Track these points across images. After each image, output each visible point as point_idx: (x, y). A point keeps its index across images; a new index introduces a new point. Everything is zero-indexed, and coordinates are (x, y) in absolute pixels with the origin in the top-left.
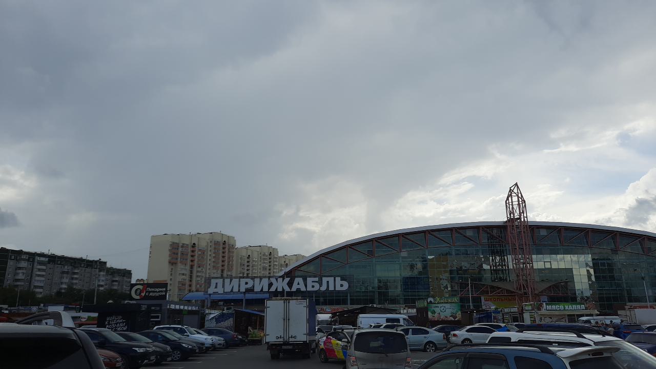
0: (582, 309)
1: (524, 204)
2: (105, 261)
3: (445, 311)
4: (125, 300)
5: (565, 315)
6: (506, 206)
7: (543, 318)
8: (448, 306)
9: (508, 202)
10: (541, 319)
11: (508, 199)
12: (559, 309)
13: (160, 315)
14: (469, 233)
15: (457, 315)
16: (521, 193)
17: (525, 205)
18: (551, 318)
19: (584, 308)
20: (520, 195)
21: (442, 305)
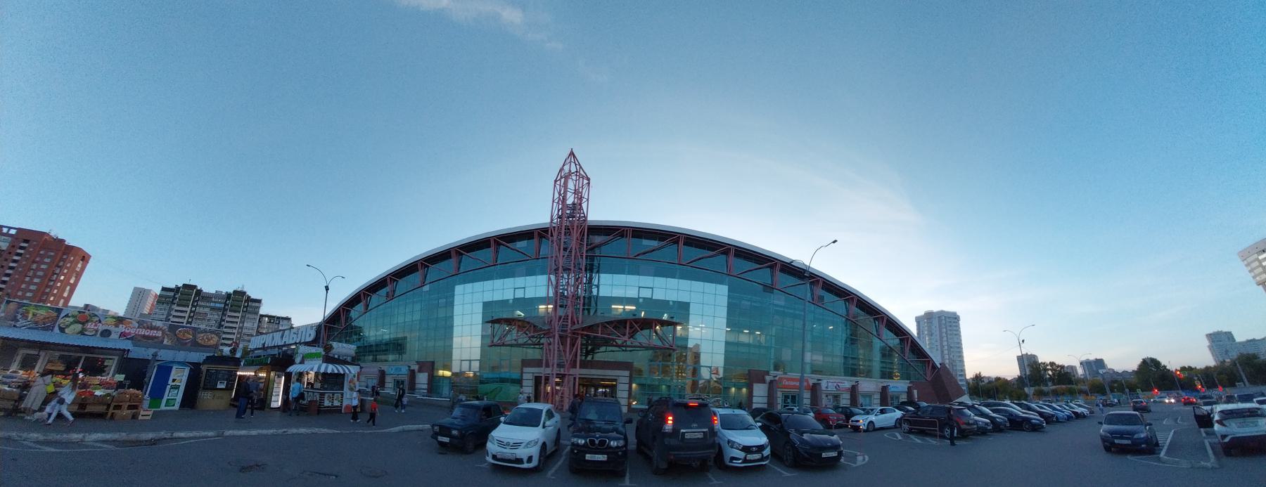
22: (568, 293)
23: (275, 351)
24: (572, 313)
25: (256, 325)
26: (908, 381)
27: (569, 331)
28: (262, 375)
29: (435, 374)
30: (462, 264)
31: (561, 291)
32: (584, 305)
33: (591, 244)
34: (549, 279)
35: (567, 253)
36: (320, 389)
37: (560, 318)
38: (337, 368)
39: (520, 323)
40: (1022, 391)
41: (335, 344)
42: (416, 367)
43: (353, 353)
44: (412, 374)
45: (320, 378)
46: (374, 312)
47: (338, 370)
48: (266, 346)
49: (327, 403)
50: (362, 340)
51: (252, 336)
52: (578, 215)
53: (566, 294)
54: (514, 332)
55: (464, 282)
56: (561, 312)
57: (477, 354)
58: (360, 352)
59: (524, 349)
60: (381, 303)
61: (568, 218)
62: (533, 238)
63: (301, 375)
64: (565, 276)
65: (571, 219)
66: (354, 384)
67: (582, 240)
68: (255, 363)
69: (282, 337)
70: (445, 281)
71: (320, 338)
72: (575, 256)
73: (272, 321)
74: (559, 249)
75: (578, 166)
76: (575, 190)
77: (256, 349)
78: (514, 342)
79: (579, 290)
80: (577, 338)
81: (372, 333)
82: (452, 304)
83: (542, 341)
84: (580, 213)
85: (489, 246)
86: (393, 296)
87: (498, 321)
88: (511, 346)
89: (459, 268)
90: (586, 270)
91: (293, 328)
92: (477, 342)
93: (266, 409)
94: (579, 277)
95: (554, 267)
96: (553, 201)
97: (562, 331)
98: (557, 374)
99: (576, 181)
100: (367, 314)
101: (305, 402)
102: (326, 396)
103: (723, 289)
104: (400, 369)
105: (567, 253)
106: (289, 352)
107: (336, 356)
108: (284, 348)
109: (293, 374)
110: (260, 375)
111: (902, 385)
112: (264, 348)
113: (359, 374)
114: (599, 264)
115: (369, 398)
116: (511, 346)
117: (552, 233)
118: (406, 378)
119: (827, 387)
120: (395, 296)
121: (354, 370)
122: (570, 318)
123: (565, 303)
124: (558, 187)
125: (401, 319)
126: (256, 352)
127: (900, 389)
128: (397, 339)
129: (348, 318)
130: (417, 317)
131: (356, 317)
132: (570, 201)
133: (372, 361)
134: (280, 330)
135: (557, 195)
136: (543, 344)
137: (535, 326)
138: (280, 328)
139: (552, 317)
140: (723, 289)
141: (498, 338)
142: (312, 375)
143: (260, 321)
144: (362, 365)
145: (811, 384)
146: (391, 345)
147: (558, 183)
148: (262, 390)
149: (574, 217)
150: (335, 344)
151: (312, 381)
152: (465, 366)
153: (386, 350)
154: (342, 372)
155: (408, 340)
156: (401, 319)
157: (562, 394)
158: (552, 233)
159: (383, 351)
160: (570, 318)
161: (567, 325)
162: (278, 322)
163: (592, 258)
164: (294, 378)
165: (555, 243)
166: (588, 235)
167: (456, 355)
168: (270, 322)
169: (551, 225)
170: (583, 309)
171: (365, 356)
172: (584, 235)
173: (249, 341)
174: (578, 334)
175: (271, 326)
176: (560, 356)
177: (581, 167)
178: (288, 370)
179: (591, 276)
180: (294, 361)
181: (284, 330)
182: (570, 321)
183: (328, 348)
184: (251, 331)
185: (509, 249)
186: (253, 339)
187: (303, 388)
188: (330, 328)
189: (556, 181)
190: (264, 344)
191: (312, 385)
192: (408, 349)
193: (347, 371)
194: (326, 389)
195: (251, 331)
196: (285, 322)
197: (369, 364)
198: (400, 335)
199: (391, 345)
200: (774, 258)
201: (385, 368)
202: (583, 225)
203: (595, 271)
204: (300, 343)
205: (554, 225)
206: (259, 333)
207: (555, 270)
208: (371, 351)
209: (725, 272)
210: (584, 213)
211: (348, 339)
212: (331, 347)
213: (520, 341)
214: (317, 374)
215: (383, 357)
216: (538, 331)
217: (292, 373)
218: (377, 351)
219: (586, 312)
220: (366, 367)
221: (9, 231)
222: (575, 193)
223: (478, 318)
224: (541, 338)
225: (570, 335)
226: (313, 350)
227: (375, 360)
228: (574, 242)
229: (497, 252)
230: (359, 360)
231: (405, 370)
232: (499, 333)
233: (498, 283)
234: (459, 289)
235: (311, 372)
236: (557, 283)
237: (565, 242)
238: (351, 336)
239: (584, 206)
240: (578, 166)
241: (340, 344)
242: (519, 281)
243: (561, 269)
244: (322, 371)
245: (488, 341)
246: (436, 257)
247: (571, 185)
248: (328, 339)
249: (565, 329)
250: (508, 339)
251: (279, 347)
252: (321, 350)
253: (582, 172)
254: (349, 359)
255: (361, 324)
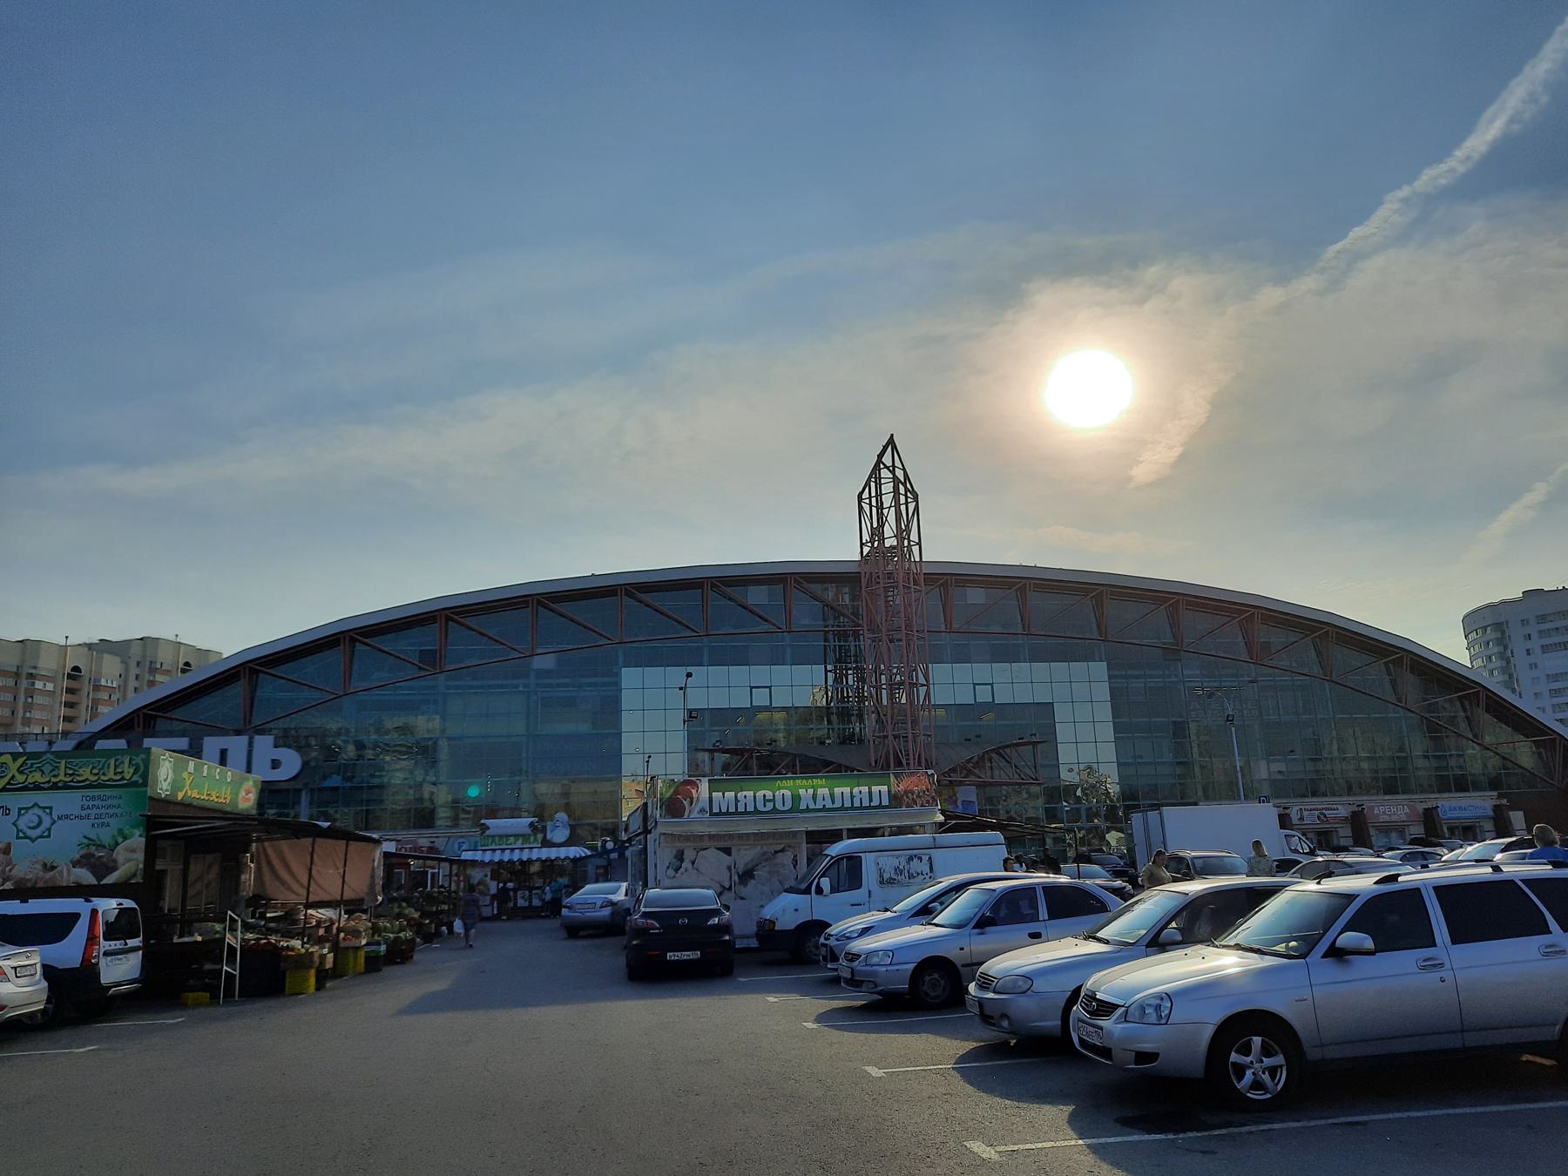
0: (875, 803)
1: (912, 507)
2: (270, 763)
3: (47, 834)
4: (1531, 853)
5: (794, 834)
6: (861, 508)
7: (689, 854)
8: (67, 802)
9: (866, 495)
10: (680, 856)
11: (868, 484)
12: (770, 806)
13: (403, 871)
14: (757, 596)
15: (120, 854)
16: (904, 469)
17: (917, 508)
18: (728, 851)
19: (885, 802)
20: (900, 474)
21: (27, 799)
26: (1495, 793)
38: (583, 851)
40: (330, 971)
47: (585, 853)
103: (1100, 669)
111: (1478, 802)
119: (1302, 819)
124: (866, 508)
127: (1479, 812)
140: (1100, 669)
145: (1421, 811)
200: (1398, 648)
209: (1020, 631)
221: (830, 671)
242: (760, 674)
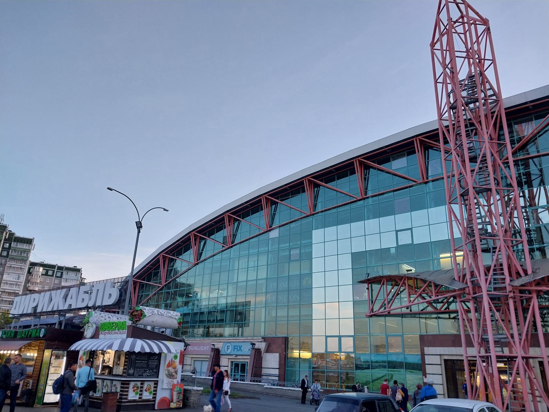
22: (493, 228)
23: (55, 319)
24: (509, 257)
25: (23, 279)
27: (509, 289)
28: (32, 355)
29: (289, 356)
30: (319, 200)
31: (480, 227)
32: (530, 242)
33: (520, 139)
34: (451, 211)
35: (477, 166)
36: (121, 376)
37: (488, 269)
39: (411, 282)
41: (147, 310)
42: (262, 346)
43: (174, 323)
44: (257, 355)
45: (123, 359)
46: (208, 263)
48: (39, 310)
49: (132, 395)
50: (190, 304)
51: (16, 295)
52: (483, 95)
53: (490, 230)
54: (404, 295)
55: (325, 225)
56: (486, 260)
57: (348, 328)
58: (187, 322)
59: (423, 321)
60: (216, 251)
61: (467, 104)
62: (414, 152)
63: (92, 354)
64: (482, 201)
65: (472, 106)
66: (175, 368)
67: (500, 137)
68: (19, 337)
69: (66, 297)
70: (298, 224)
71: (124, 300)
72: (494, 166)
73: (50, 273)
74: (463, 161)
75: (462, 7)
76: (467, 51)
77: (22, 315)
78: (404, 310)
79: (516, 220)
80: (531, 298)
81: (205, 295)
82: (309, 257)
83: (452, 307)
84: (484, 91)
85: (353, 172)
86: (233, 242)
87: (378, 280)
88: (402, 315)
89: (315, 206)
90: (520, 184)
91: (84, 284)
92: (348, 311)
93: (37, 405)
94: (510, 199)
95: (458, 191)
96: (436, 82)
97: (495, 289)
98: (498, 357)
99: (465, 34)
100: (200, 265)
101: (98, 394)
102: (132, 384)
104: (240, 347)
105: (477, 166)
106: (76, 321)
107: (149, 328)
108: (68, 315)
109: (81, 354)
110: (28, 354)
112: (35, 314)
113: (183, 355)
114: (541, 170)
115: (195, 388)
116: (402, 315)
117: (445, 138)
118: (248, 360)
120: (236, 242)
121: (175, 347)
122: (505, 267)
123: (491, 245)
124: (438, 53)
125: (242, 278)
126: (22, 319)
128: (236, 305)
129: (171, 271)
130: (263, 274)
131: (184, 269)
132: (463, 75)
133: (203, 336)
134: (63, 287)
135: (439, 69)
136: (456, 312)
137: (436, 286)
138: (63, 284)
139: (464, 269)
141: (379, 305)
142: (110, 357)
143: (29, 273)
144: (188, 340)
146: (228, 313)
147: (438, 46)
148: (29, 377)
149: (477, 100)
150: (147, 310)
151: (111, 364)
152: (333, 345)
153: (222, 320)
154: (157, 351)
155: (252, 306)
156: (242, 278)
157: (513, 386)
158: (445, 138)
159: (217, 321)
160: (505, 267)
161: (504, 279)
162: (59, 274)
163: (526, 163)
164: (82, 358)
165: (454, 153)
166: (510, 126)
167: (317, 328)
168: (46, 274)
169: (440, 124)
170: (532, 251)
171: (194, 327)
172: (501, 128)
173: (11, 303)
174: (530, 292)
175: (48, 280)
176: (497, 329)
177: (468, 6)
178: (73, 348)
179: (531, 193)
180: (83, 333)
181: (69, 288)
182: (506, 271)
183: (136, 316)
184: (15, 288)
185: (384, 174)
186: (17, 299)
187: (95, 374)
188: (142, 286)
189: (433, 45)
190: (35, 308)
191: (110, 369)
192: (251, 319)
193: (165, 350)
194: (133, 375)
195: (15, 288)
196: (72, 275)
197: (198, 340)
198: (241, 300)
199: (228, 313)
201: (218, 345)
202: (497, 109)
203: (535, 183)
204: (94, 308)
205: (446, 123)
206: (27, 291)
207: (462, 195)
208: (201, 322)
210: (492, 88)
211: (169, 302)
212: (141, 315)
213: (415, 309)
214: (118, 354)
215: (218, 330)
216: (442, 293)
217: (78, 352)
218: (209, 321)
219: (537, 254)
220: (196, 345)
222: (468, 57)
223: (347, 277)
224: (449, 304)
225: (511, 295)
226: (113, 318)
227: (207, 334)
228: (487, 145)
229: (366, 179)
230: (185, 333)
231: (247, 349)
232: (381, 297)
233: (372, 224)
234: (317, 235)
235: (109, 351)
236: (470, 215)
237: (469, 149)
238: (174, 299)
239: (490, 74)
240: (462, 7)
241: (156, 310)
243: (471, 191)
244: (126, 348)
245: (366, 310)
246: (286, 190)
247: (459, 45)
248: (138, 303)
249: (503, 285)
250: (396, 306)
251: (61, 313)
252: (125, 319)
253: (472, 14)
254: (168, 332)
255: (191, 281)
